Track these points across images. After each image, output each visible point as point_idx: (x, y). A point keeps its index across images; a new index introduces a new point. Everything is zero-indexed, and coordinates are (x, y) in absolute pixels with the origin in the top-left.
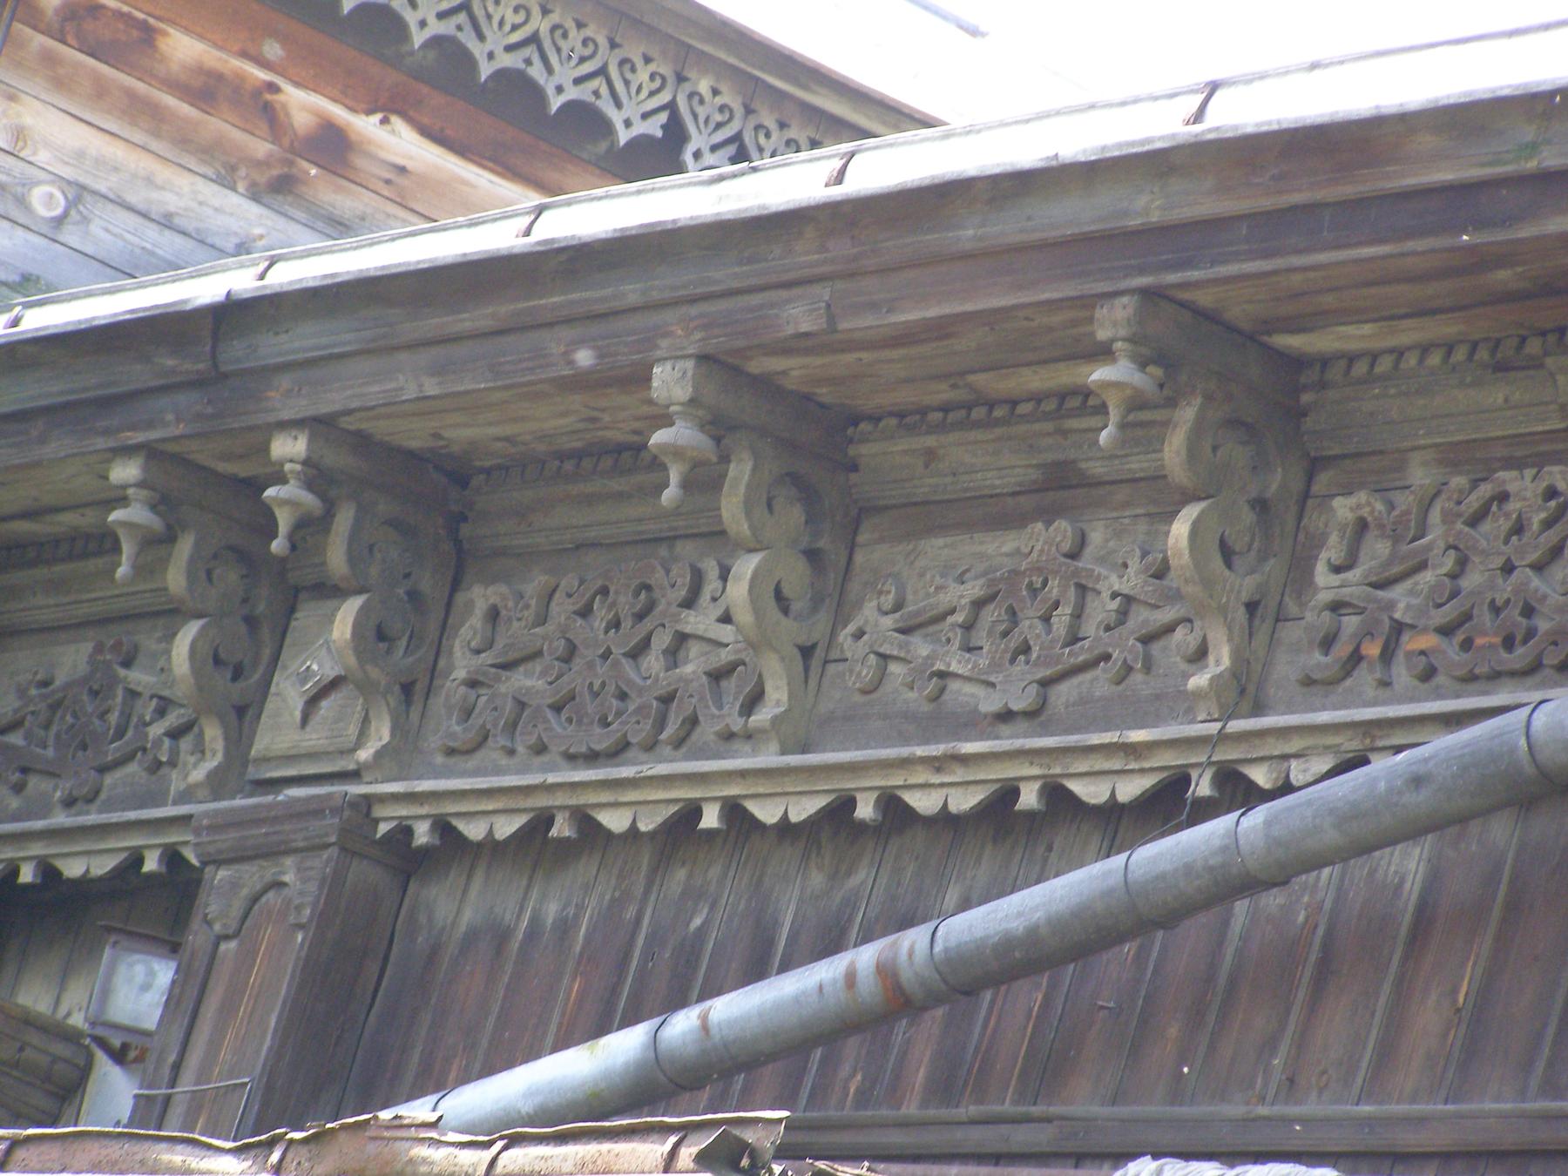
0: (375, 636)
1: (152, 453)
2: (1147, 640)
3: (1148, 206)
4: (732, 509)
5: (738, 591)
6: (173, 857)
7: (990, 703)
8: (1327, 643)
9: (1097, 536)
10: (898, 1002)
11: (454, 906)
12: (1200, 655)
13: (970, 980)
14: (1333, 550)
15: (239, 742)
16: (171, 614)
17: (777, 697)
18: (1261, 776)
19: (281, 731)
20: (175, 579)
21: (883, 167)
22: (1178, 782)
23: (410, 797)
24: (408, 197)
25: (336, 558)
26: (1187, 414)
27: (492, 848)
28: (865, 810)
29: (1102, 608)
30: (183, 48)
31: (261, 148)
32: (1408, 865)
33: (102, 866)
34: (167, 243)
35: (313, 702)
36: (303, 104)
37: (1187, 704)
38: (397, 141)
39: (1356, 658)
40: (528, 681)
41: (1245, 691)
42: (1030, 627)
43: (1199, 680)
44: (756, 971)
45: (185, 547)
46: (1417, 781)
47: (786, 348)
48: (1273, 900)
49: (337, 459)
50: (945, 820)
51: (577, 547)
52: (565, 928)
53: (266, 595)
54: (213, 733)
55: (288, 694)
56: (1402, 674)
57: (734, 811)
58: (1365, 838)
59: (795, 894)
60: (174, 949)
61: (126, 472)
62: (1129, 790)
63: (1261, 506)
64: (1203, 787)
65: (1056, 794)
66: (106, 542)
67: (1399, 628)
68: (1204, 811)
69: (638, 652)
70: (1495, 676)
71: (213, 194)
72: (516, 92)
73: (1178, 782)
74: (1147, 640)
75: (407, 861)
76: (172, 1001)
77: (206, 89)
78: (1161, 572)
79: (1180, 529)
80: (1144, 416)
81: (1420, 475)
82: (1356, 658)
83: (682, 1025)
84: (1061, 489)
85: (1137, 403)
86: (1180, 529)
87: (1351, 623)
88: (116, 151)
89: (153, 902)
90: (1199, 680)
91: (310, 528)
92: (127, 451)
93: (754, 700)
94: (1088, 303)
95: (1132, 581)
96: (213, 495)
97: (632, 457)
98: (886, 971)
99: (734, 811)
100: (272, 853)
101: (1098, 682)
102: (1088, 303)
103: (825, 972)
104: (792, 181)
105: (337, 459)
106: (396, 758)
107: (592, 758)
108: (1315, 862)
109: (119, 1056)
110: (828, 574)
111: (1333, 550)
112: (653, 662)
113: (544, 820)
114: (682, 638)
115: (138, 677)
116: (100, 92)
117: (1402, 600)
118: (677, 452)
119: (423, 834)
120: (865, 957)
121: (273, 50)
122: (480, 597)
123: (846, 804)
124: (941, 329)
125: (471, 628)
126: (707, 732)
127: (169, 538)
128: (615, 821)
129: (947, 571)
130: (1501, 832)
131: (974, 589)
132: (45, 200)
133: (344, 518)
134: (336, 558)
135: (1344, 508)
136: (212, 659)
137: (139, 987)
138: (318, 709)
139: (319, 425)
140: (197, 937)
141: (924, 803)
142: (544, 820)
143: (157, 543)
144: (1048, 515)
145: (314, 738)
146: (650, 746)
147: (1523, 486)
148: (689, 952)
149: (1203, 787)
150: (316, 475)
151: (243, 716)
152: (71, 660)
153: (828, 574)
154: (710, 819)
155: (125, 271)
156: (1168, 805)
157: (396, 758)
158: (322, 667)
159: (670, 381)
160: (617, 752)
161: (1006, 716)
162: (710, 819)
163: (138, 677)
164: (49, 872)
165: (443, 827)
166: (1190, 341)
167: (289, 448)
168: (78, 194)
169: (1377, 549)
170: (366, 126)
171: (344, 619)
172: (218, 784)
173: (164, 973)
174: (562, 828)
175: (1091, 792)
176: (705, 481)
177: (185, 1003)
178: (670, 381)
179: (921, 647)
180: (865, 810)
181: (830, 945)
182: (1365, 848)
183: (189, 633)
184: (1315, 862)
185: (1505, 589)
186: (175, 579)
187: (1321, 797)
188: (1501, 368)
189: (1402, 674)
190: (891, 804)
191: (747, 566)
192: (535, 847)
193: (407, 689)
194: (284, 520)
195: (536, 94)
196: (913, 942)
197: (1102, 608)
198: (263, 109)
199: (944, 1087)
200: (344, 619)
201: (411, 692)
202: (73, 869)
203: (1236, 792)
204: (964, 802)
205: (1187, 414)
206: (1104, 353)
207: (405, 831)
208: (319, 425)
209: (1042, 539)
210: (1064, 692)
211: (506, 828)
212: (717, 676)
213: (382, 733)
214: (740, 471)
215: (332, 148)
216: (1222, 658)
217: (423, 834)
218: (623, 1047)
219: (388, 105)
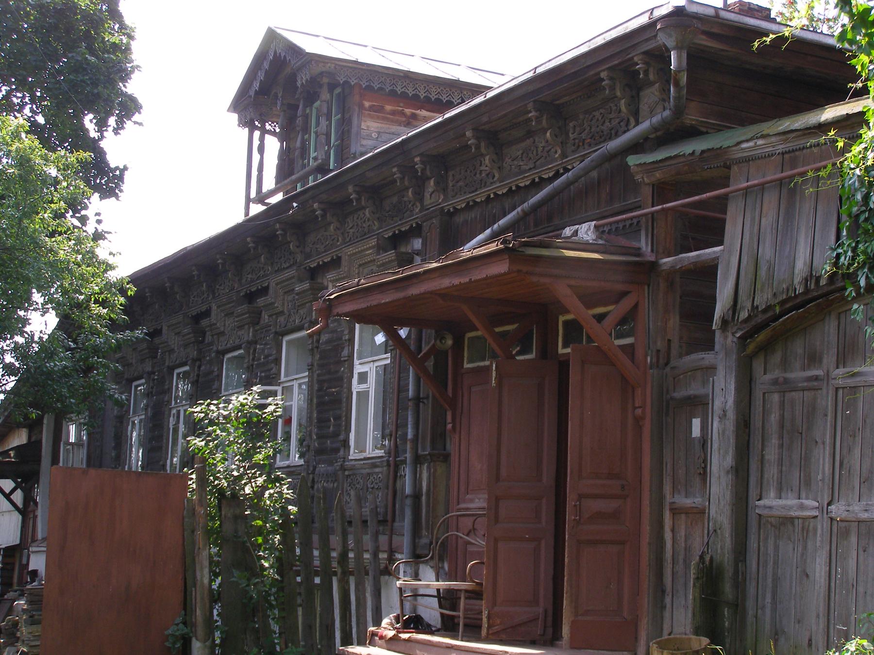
0: (437, 183)
1: (398, 166)
2: (548, 152)
3: (531, 88)
4: (483, 150)
5: (487, 161)
6: (417, 223)
7: (527, 168)
8: (574, 145)
9: (537, 139)
10: (526, 214)
11: (459, 219)
12: (556, 152)
13: (535, 208)
14: (571, 131)
15: (422, 205)
16: (407, 188)
17: (497, 175)
18: (569, 167)
19: (427, 201)
20: (406, 183)
21: (490, 95)
22: (558, 171)
23: (447, 206)
24: (426, 120)
25: (428, 173)
26: (545, 117)
27: (462, 209)
28: (514, 188)
29: (540, 149)
30: (388, 108)
31: (404, 119)
32: (594, 174)
33: (407, 228)
34: (391, 136)
35: (431, 195)
36: (408, 111)
37: (556, 160)
38: (424, 113)
39: (579, 146)
40: (460, 183)
41: (564, 155)
42: (530, 155)
43: (557, 156)
44: (505, 216)
45: (406, 178)
46: (592, 161)
47: (484, 124)
48: (576, 184)
49: (357, 189)
50: (526, 186)
51: (185, 609)
52: (476, 218)
53: (420, 183)
54: (418, 204)
55: (427, 195)
56: (586, 146)
57: (495, 194)
58: (587, 171)
59: (507, 204)
60: (421, 237)
61: (395, 170)
62: (551, 175)
63: (559, 128)
64: (562, 171)
65: (541, 178)
66: (395, 181)
67: (584, 140)
68: (563, 174)
69: (475, 175)
70: (600, 143)
71: (398, 128)
72: (438, 101)
73: (558, 171)
74: (548, 152)
75: (451, 214)
76: (422, 244)
77: (393, 113)
78: (547, 141)
79: (548, 134)
80: (538, 119)
81: (581, 117)
82: (579, 146)
83: (496, 226)
84: (530, 134)
85: (537, 118)
86: (548, 134)
87: (577, 141)
88: (383, 125)
89: (416, 231)
90: (557, 156)
91: (423, 170)
92: (394, 167)
93: (494, 176)
94: (526, 105)
95: (543, 144)
96: (408, 170)
97: (467, 147)
98: (523, 210)
99: (495, 194)
100: (431, 218)
101: (542, 160)
102: (526, 105)
103: (514, 213)
104: (479, 100)
105: (357, 189)
106: (444, 200)
107: (473, 192)
108: (580, 177)
109: (417, 254)
110: (499, 156)
111: (571, 131)
112: (478, 175)
113: (468, 203)
114: (481, 171)
115: (405, 199)
116: (378, 118)
117: (583, 136)
118: (472, 144)
119: (452, 210)
120: (519, 209)
121: (402, 105)
122: (451, 173)
123: (511, 188)
124: (505, 115)
125: (450, 178)
126: (488, 183)
127: (404, 178)
128: (478, 200)
129: (516, 151)
130: (607, 165)
131: (521, 152)
132: (374, 135)
133: (428, 167)
134: (428, 173)
135: (571, 125)
136: (415, 193)
137: (417, 244)
138: (432, 197)
139: (421, 155)
140: (424, 234)
141: (522, 185)
142: (468, 203)
143: (402, 179)
144: (529, 138)
145: (433, 200)
146: (481, 188)
147: (597, 114)
148: (494, 216)
149: (562, 171)
150: (422, 162)
151: (421, 200)
152: (395, 199)
153: (499, 156)
154: (492, 196)
155: (386, 142)
156: (557, 175)
157: (444, 200)
158: (431, 190)
159: (469, 134)
160: (476, 190)
161: (530, 169)
162: (492, 196)
163: (405, 199)
164: (400, 231)
165: (454, 208)
166: (543, 107)
167: (417, 159)
168: (379, 133)
169: (578, 129)
170: (418, 112)
171: (432, 182)
172: (421, 211)
173: (420, 241)
174: (471, 203)
175: (546, 176)
176: (478, 147)
177: (424, 244)
178: (469, 134)
179: (516, 162)
180: (514, 188)
181: (514, 208)
182: (587, 173)
183: (410, 190)
184: (580, 177)
185: (598, 129)
186: (406, 183)
187: (579, 167)
188: (589, 97)
189: (586, 146)
190: (517, 186)
191: (487, 158)
192: (468, 208)
193: (444, 190)
194: (419, 170)
195: (442, 101)
196: (526, 204)
197: (540, 149)
198: (402, 114)
199: (536, 225)
200: (432, 182)
201: (445, 190)
202: (403, 229)
203: (567, 170)
204: (528, 183)
205: (545, 117)
206: (530, 112)
207: (449, 210)
208: (421, 155)
209: (529, 142)
210: (538, 163)
211: (463, 206)
212: (487, 175)
213: (442, 197)
214: (483, 144)
215: (414, 117)
216: (559, 152)
217: (452, 210)
218: (488, 232)
219: (421, 108)
